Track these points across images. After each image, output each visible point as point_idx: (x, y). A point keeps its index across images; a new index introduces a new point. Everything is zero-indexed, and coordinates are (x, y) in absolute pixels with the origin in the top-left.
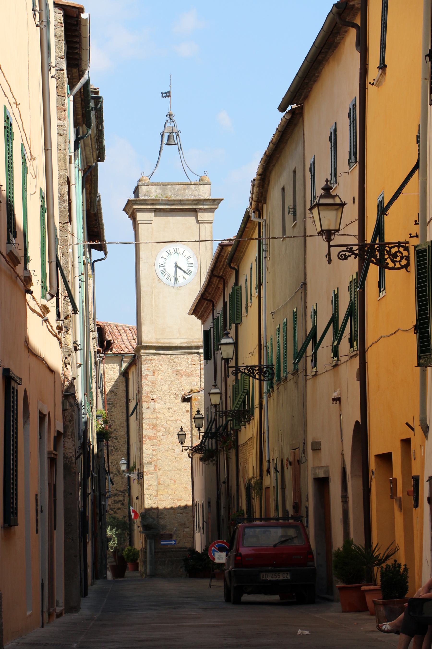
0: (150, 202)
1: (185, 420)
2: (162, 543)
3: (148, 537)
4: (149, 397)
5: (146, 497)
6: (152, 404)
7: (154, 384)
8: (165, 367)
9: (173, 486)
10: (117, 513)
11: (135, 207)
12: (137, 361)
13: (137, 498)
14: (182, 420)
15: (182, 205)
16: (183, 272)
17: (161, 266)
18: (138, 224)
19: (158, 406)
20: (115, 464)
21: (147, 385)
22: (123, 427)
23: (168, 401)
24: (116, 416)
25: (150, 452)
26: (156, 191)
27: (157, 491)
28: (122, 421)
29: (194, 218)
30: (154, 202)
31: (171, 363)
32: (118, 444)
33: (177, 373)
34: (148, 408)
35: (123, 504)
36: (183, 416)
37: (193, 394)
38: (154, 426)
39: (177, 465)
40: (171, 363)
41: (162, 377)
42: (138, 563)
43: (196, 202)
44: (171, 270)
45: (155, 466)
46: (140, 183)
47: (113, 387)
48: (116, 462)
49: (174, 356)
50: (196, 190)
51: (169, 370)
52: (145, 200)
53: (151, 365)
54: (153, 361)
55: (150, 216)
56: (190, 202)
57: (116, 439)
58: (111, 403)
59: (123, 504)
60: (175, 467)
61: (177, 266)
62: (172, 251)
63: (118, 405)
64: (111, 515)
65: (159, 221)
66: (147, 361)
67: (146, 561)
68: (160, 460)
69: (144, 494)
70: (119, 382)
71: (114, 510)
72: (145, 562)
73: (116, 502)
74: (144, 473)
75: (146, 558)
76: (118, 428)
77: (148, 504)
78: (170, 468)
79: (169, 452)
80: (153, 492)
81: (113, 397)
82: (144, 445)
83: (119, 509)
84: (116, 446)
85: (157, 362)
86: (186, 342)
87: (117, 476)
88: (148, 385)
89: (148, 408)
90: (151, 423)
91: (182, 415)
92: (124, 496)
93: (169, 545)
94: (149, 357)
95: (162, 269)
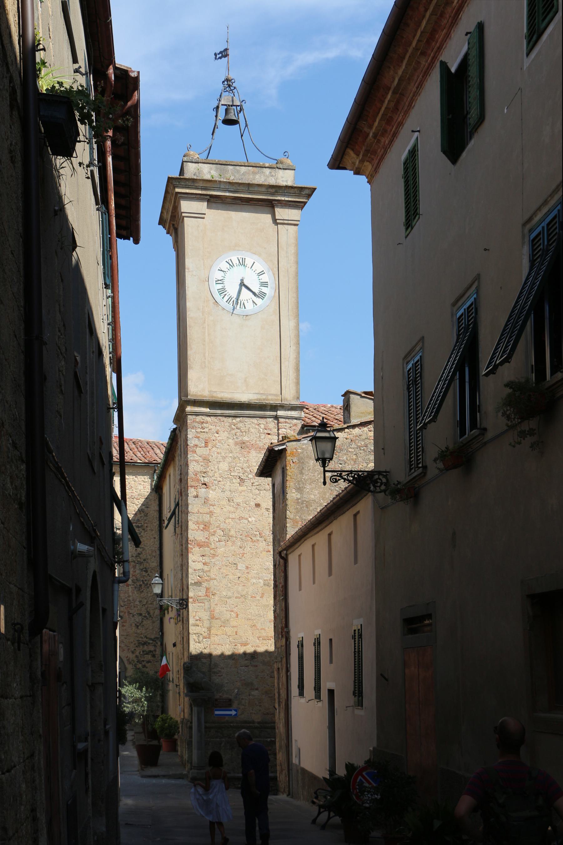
0: (201, 184)
1: (253, 519)
2: (217, 713)
3: (194, 702)
4: (198, 480)
5: (192, 638)
6: (202, 491)
7: (206, 460)
8: (223, 435)
9: (234, 623)
10: (147, 667)
11: (177, 190)
12: (179, 437)
13: (174, 645)
14: (250, 519)
15: (250, 193)
16: (251, 294)
17: (218, 282)
18: (184, 217)
19: (212, 494)
20: (145, 603)
21: (196, 461)
23: (227, 488)
25: (200, 566)
26: (210, 172)
27: (209, 629)
28: (154, 549)
29: (269, 216)
30: (208, 185)
31: (233, 429)
33: (243, 445)
34: (197, 496)
35: (154, 656)
36: (250, 513)
37: (287, 444)
38: (206, 526)
39: (240, 589)
40: (233, 429)
41: (219, 451)
42: (176, 740)
43: (273, 190)
44: (232, 290)
45: (207, 589)
46: (185, 159)
47: (143, 505)
48: (145, 601)
49: (238, 419)
50: (272, 176)
51: (230, 441)
52: (193, 180)
53: (202, 431)
54: (205, 425)
55: (201, 206)
56: (263, 189)
57: (146, 571)
58: (140, 525)
59: (154, 656)
60: (238, 592)
61: (242, 284)
62: (235, 261)
63: (149, 528)
64: (139, 669)
65: (216, 216)
66: (196, 424)
67: (192, 741)
68: (215, 579)
69: (189, 633)
70: (150, 500)
71: (143, 663)
72: (190, 744)
73: (145, 653)
74: (190, 600)
75: (191, 737)
76: (149, 557)
77: (195, 648)
78: (230, 594)
79: (228, 568)
80: (203, 630)
82: (190, 555)
83: (149, 662)
84: (146, 580)
85: (211, 427)
86: (257, 400)
87: (147, 619)
88: (197, 461)
89: (197, 496)
90: (201, 520)
91: (249, 511)
92: (155, 646)
93: (227, 718)
94: (199, 418)
95: (220, 286)
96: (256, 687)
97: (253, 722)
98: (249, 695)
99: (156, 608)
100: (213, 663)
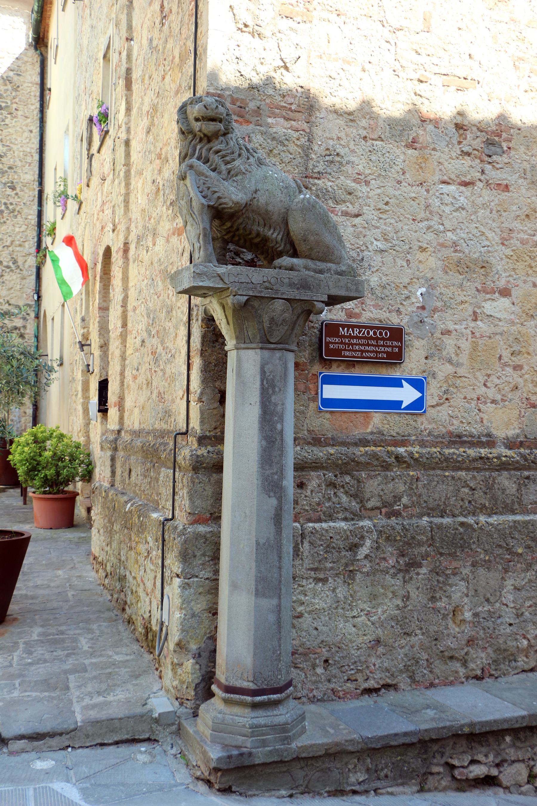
20: (8, 244)
22: (30, 164)
24: (14, 136)
28: (28, 150)
32: (16, 199)
48: (9, 240)
57: (13, 188)
63: (20, 113)
76: (19, 164)
81: (9, 92)
84: (11, 204)
87: (12, 271)
96: (502, 283)
97: (490, 442)
98: (475, 317)
99: (30, 254)
100: (318, 148)
